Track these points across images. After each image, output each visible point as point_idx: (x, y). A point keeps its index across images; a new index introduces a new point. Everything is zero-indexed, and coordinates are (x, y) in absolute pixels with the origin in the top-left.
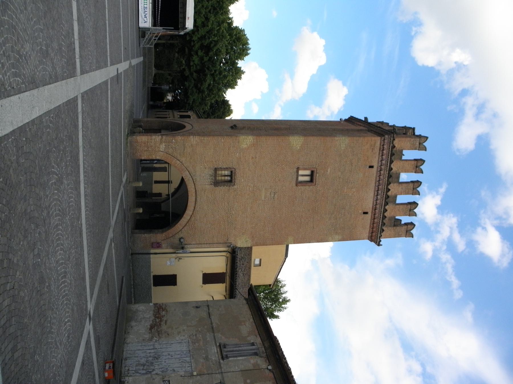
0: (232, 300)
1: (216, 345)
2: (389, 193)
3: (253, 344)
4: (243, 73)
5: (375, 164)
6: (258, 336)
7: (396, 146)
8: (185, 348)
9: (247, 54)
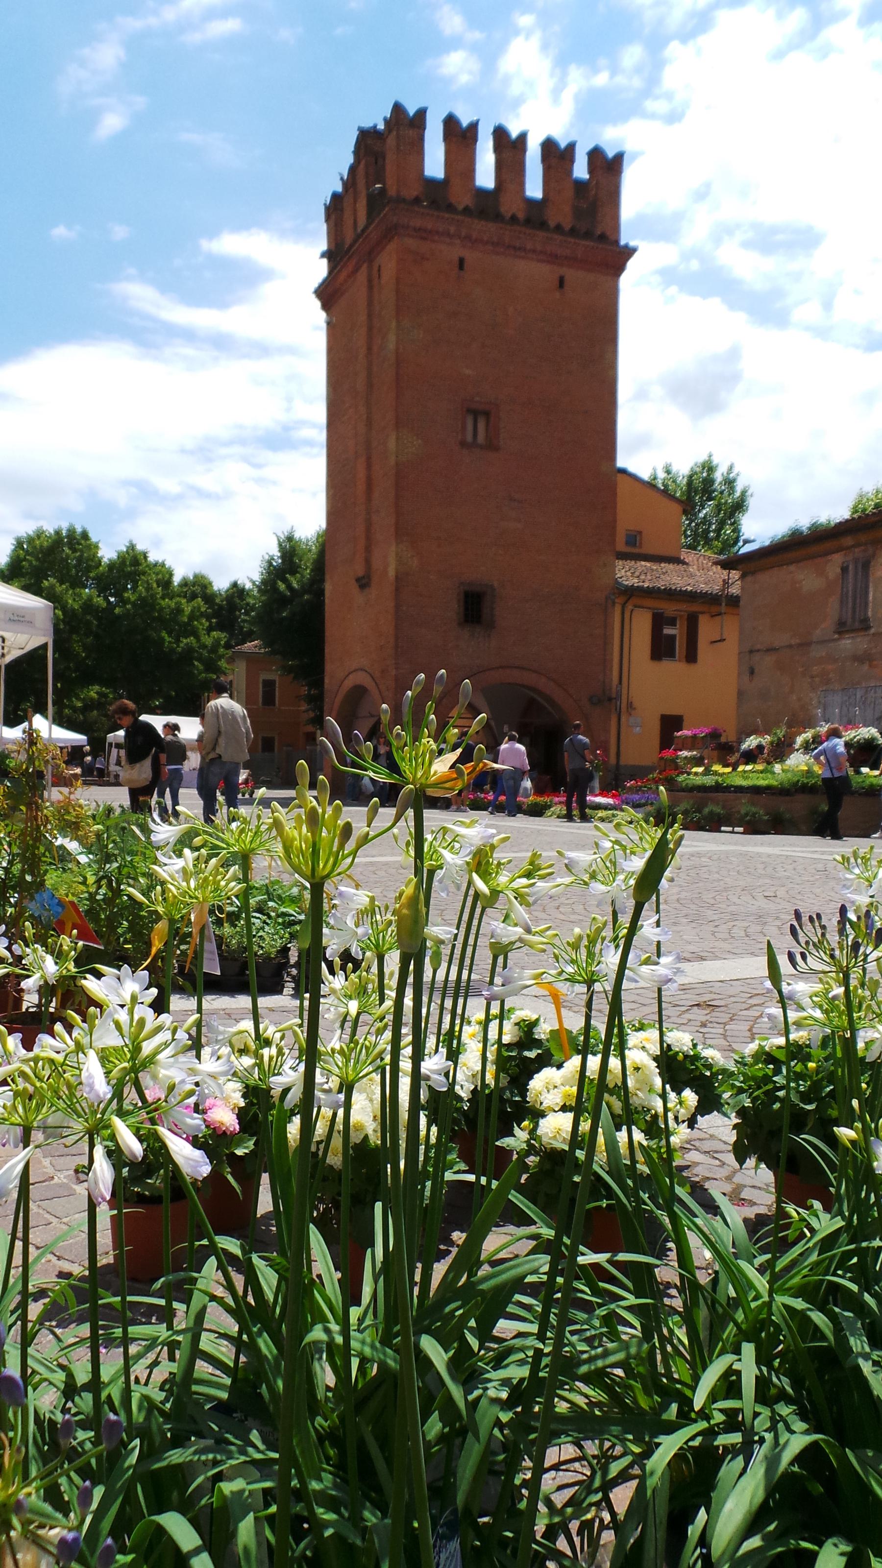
0: (742, 603)
1: (838, 639)
2: (521, 216)
3: (844, 570)
4: (132, 547)
5: (453, 252)
6: (829, 557)
7: (415, 193)
8: (837, 698)
9: (85, 535)
